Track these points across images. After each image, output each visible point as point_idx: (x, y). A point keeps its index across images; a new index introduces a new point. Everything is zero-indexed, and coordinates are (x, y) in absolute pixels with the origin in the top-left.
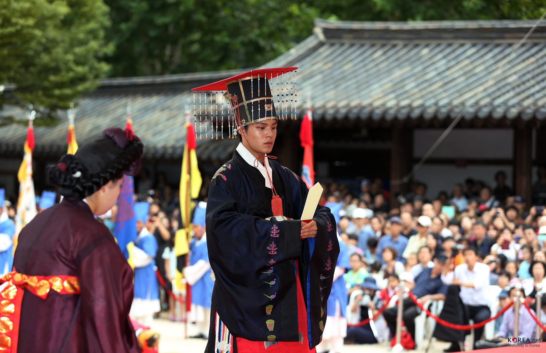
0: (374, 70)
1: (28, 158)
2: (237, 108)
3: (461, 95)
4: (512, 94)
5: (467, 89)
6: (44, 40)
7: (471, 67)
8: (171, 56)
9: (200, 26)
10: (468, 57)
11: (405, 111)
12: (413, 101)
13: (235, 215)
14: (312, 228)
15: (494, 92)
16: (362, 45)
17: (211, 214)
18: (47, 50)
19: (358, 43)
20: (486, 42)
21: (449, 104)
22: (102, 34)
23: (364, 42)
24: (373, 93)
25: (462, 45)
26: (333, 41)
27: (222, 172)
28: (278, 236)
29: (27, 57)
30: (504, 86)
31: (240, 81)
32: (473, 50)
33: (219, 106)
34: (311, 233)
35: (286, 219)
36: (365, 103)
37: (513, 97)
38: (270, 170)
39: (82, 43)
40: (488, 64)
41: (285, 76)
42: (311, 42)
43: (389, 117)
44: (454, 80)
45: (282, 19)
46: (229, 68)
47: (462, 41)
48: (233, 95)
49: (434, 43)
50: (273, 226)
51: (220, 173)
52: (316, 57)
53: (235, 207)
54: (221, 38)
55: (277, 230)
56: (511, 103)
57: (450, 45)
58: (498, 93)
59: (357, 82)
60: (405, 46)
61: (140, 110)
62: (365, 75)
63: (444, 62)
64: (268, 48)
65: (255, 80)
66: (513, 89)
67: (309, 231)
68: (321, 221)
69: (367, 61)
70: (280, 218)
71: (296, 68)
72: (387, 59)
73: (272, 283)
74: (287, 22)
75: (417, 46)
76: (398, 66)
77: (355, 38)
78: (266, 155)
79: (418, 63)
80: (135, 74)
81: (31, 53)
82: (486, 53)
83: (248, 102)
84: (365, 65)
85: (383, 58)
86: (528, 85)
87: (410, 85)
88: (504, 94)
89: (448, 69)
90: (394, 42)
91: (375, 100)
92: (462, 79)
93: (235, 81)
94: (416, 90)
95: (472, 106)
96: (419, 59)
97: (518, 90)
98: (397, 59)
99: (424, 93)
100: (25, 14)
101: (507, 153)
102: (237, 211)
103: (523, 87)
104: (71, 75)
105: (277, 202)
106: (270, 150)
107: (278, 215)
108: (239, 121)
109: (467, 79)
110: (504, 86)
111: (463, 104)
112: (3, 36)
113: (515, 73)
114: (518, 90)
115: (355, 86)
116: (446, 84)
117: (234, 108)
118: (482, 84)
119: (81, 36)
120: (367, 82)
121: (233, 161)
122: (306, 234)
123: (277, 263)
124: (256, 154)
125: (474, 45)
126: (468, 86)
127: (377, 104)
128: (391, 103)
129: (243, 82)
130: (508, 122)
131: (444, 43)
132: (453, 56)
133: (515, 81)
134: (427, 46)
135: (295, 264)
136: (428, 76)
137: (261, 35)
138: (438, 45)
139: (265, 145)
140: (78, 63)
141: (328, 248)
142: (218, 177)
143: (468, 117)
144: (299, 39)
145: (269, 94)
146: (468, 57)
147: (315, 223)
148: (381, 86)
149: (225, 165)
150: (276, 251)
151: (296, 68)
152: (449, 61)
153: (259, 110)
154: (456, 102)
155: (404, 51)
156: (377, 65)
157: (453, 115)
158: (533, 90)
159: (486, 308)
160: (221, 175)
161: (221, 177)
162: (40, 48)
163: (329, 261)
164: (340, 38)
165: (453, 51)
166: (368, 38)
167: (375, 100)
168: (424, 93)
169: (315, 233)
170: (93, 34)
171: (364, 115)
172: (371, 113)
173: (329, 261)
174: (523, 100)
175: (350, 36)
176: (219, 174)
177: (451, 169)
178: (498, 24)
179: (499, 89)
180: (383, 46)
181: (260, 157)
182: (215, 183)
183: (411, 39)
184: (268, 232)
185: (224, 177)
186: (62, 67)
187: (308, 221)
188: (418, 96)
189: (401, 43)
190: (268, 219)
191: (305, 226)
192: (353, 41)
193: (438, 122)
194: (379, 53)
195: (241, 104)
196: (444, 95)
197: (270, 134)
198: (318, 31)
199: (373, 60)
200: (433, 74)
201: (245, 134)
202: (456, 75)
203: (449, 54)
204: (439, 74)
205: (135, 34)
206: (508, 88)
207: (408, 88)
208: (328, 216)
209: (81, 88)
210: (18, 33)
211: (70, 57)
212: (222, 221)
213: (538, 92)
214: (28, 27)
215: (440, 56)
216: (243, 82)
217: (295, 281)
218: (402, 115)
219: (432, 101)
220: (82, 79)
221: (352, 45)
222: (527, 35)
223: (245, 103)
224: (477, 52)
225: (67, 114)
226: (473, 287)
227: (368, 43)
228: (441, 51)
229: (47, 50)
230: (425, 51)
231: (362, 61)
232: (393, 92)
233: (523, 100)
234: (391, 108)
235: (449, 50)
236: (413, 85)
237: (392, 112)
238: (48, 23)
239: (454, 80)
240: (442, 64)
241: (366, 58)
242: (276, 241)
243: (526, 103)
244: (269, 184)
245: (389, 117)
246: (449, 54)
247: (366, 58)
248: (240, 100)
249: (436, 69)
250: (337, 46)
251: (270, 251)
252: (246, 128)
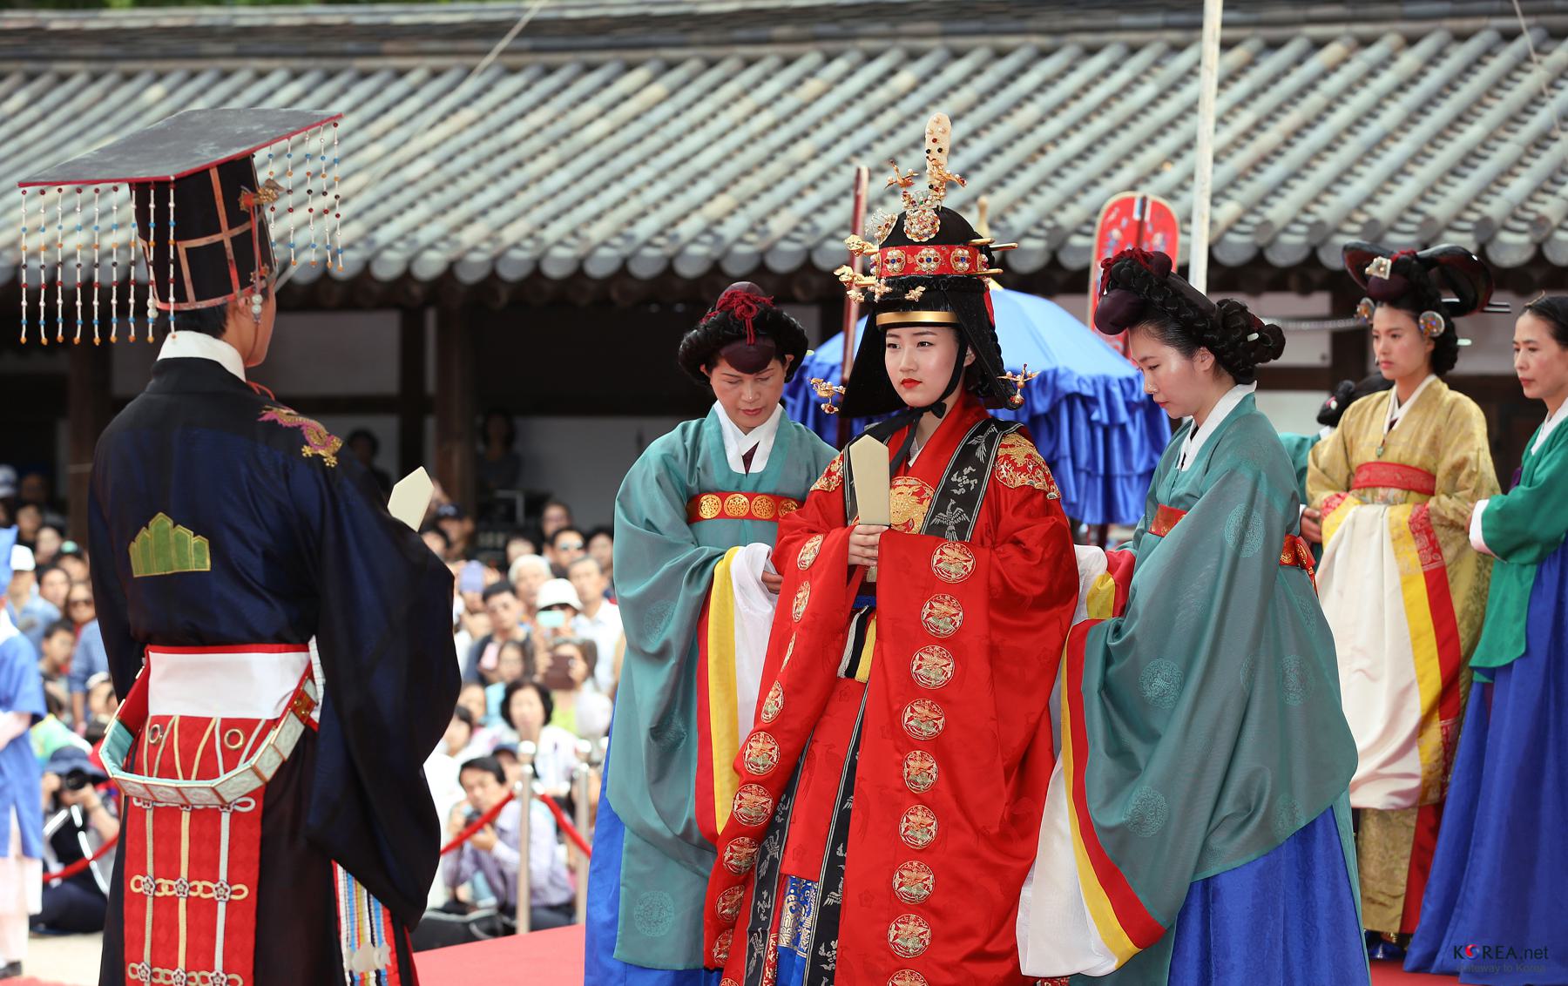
4: (422, 210)
25: (261, 75)
43: (644, 269)
47: (261, 64)
49: (178, 70)
56: (425, 235)
86: (466, 184)
97: (438, 200)
101: (385, 378)
103: (452, 193)
110: (398, 191)
114: (438, 200)
131: (771, 56)
158: (481, 201)
174: (458, 228)
206: (409, 194)
213: (498, 204)
222: (503, 44)
223: (225, 236)
233: (458, 228)
243: (469, 236)
246: (435, 100)
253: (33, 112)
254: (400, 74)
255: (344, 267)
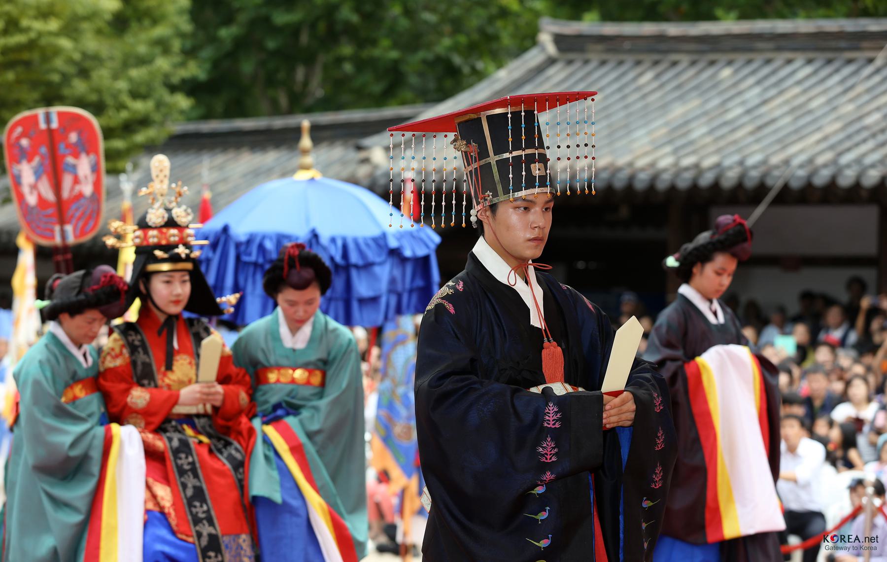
0: (639, 105)
1: (26, 259)
2: (476, 169)
3: (784, 147)
4: (870, 144)
5: (794, 137)
6: (77, 56)
7: (802, 99)
8: (306, 84)
9: (350, 31)
10: (799, 83)
11: (688, 176)
12: (703, 158)
13: (475, 383)
14: (625, 408)
15: (841, 142)
16: (621, 63)
17: (426, 380)
18: (84, 73)
19: (613, 58)
20: (830, 55)
21: (764, 162)
22: (176, 45)
23: (622, 57)
24: (636, 145)
25: (789, 62)
26: (571, 56)
27: (446, 298)
28: (557, 425)
29: (49, 84)
30: (858, 132)
31: (483, 116)
32: (808, 70)
33: (376, 167)
34: (624, 416)
35: (570, 389)
36: (622, 161)
37: (873, 150)
38: (539, 292)
39: (142, 61)
40: (832, 94)
41: (579, 105)
42: (533, 58)
44: (773, 121)
45: (491, 19)
46: (403, 103)
48: (468, 143)
49: (741, 58)
50: (547, 405)
51: (442, 298)
52: (541, 84)
53: (472, 367)
54: (385, 51)
55: (557, 412)
56: (868, 160)
57: (768, 62)
58: (848, 144)
59: (609, 126)
60: (693, 63)
61: (245, 175)
62: (622, 114)
63: (757, 90)
64: (466, 70)
65: (516, 115)
66: (874, 136)
67: (619, 412)
68: (641, 392)
69: (627, 91)
70: (560, 389)
71: (594, 94)
72: (661, 86)
73: (543, 516)
74: (499, 24)
75: (712, 63)
76: (680, 98)
77: (608, 51)
78: (530, 262)
79: (713, 92)
80: (242, 112)
81: (56, 78)
82: (830, 75)
83: (497, 158)
84: (624, 97)
85: (655, 84)
87: (699, 131)
88: (857, 145)
89: (765, 102)
90: (674, 57)
91: (638, 157)
92: (788, 119)
93: (473, 116)
94: (708, 139)
95: (801, 166)
96: (715, 86)
98: (679, 87)
99: (722, 143)
100: (44, 14)
101: (869, 246)
102: (477, 375)
104: (124, 115)
105: (552, 355)
106: (538, 253)
107: (553, 381)
108: (481, 195)
109: (797, 119)
110: (858, 132)
111: (787, 162)
112: (7, 50)
113: (878, 109)
115: (605, 133)
116: (759, 128)
117: (470, 168)
118: (819, 129)
119: (142, 49)
120: (626, 126)
121: (467, 273)
122: (613, 419)
123: (557, 479)
124: (512, 259)
125: (810, 62)
126: (796, 131)
127: (641, 163)
128: (665, 162)
129: (489, 118)
130: (864, 194)
131: (759, 59)
132: (773, 80)
133: (877, 123)
134: (730, 63)
135: (590, 479)
136: (730, 116)
137: (455, 48)
138: (749, 62)
139: (531, 243)
140: (135, 95)
141: (656, 444)
142: (438, 306)
143: (795, 184)
144: (522, 50)
145: (541, 145)
146: (799, 83)
147: (631, 396)
148: (650, 133)
149: (450, 283)
150: (556, 454)
151: (594, 94)
152: (766, 90)
153: (519, 175)
154: (775, 160)
155: (691, 72)
156: (644, 96)
157: (769, 182)
159: (820, 515)
160: (443, 302)
161: (445, 307)
162: (71, 70)
163: (658, 470)
164: (581, 50)
165: (774, 72)
166: (630, 51)
167: (638, 157)
168: (722, 143)
169: (632, 416)
170: (163, 45)
171: (619, 183)
172: (632, 178)
173: (658, 470)
175: (600, 47)
176: (440, 301)
177: (774, 273)
178: (850, 25)
179: (849, 137)
180: (656, 63)
181: (519, 265)
182: (432, 319)
183: (702, 52)
184: (539, 416)
185: (450, 307)
186: (109, 101)
187: (616, 394)
188: (712, 148)
189: (685, 59)
190: (536, 390)
191: (610, 403)
192: (605, 56)
193: (746, 195)
194: (649, 75)
195: (482, 162)
196: (756, 147)
197: (540, 221)
198: (545, 38)
199: (638, 89)
200: (739, 111)
201: (491, 220)
202: (778, 113)
203: (766, 77)
204: (748, 112)
205: (241, 45)
206: (865, 134)
207: (695, 135)
208: (653, 381)
209: (140, 137)
210: (31, 45)
211: (122, 85)
212: (446, 396)
214: (51, 34)
215: (751, 80)
216: (489, 118)
217: (590, 514)
218: (683, 183)
219: (736, 158)
220: (144, 122)
221: (603, 63)
223: (493, 159)
224: (815, 72)
225: (118, 182)
226: (795, 481)
227: (630, 59)
228: (753, 72)
229: (84, 73)
230: (726, 72)
231: (620, 89)
232: (670, 142)
234: (665, 170)
235: (766, 70)
236: (704, 130)
237: (666, 177)
238: (85, 25)
239: (773, 121)
240: (753, 95)
241: (626, 85)
242: (556, 435)
244: (536, 320)
245: (662, 185)
246: (766, 77)
247: (626, 85)
248: (483, 153)
249: (743, 103)
250: (577, 65)
251: (543, 455)
252: (493, 208)
253: (616, 86)
254: (871, 61)
255: (822, 178)
